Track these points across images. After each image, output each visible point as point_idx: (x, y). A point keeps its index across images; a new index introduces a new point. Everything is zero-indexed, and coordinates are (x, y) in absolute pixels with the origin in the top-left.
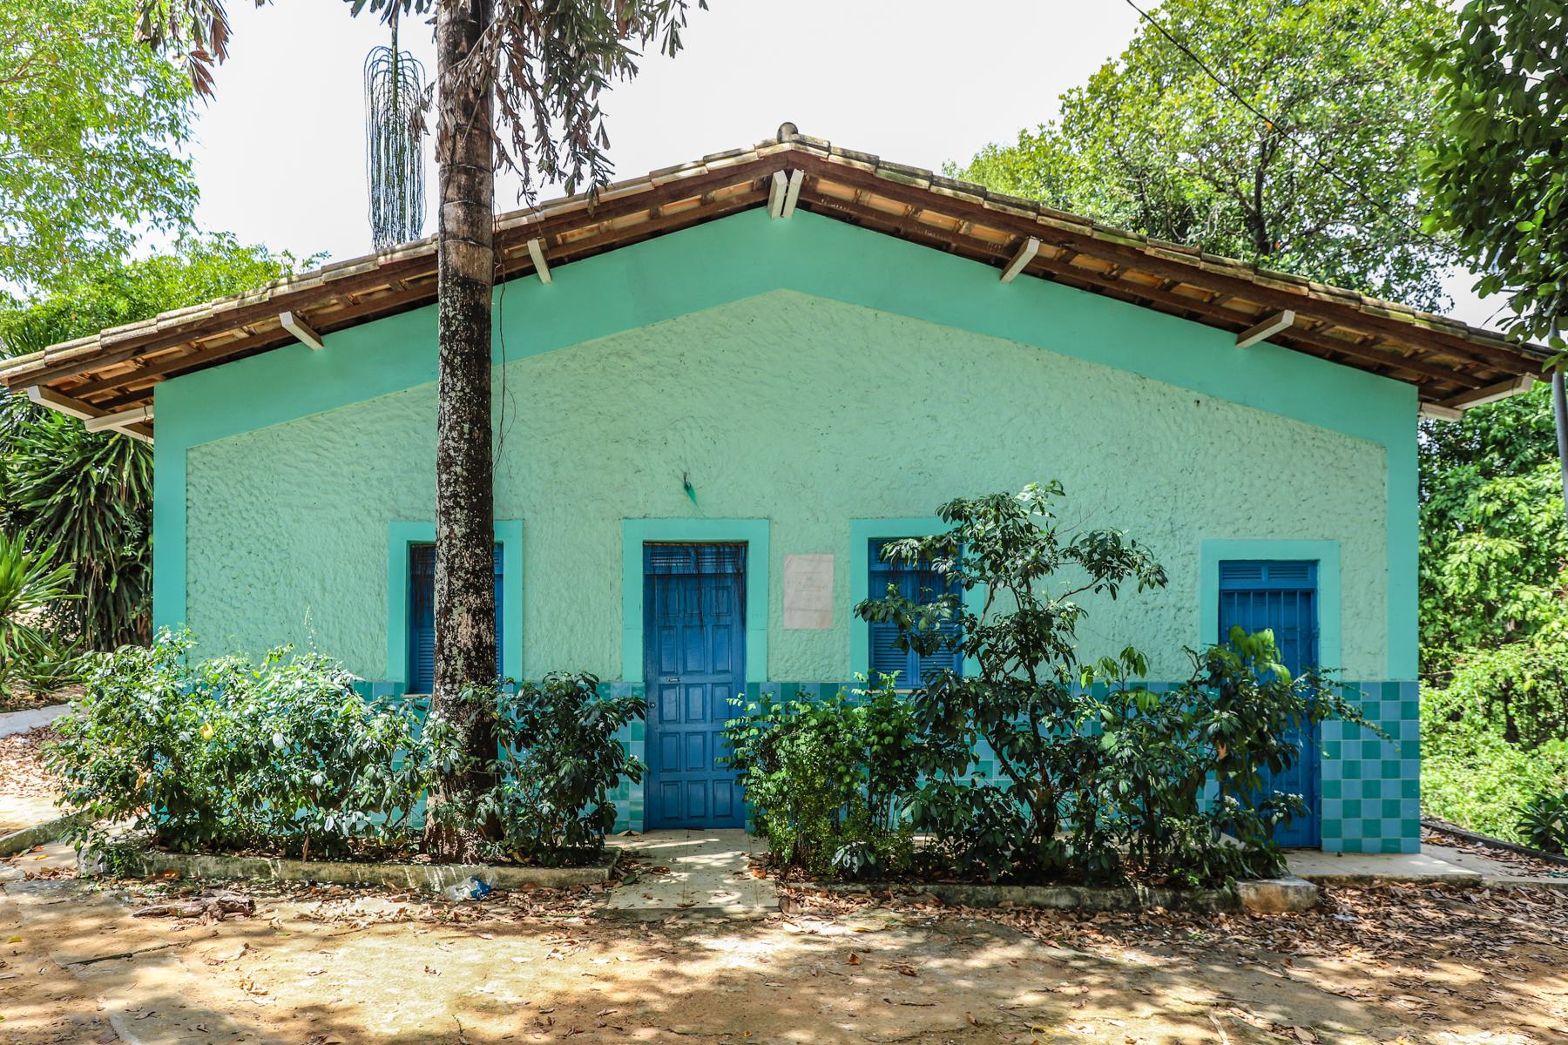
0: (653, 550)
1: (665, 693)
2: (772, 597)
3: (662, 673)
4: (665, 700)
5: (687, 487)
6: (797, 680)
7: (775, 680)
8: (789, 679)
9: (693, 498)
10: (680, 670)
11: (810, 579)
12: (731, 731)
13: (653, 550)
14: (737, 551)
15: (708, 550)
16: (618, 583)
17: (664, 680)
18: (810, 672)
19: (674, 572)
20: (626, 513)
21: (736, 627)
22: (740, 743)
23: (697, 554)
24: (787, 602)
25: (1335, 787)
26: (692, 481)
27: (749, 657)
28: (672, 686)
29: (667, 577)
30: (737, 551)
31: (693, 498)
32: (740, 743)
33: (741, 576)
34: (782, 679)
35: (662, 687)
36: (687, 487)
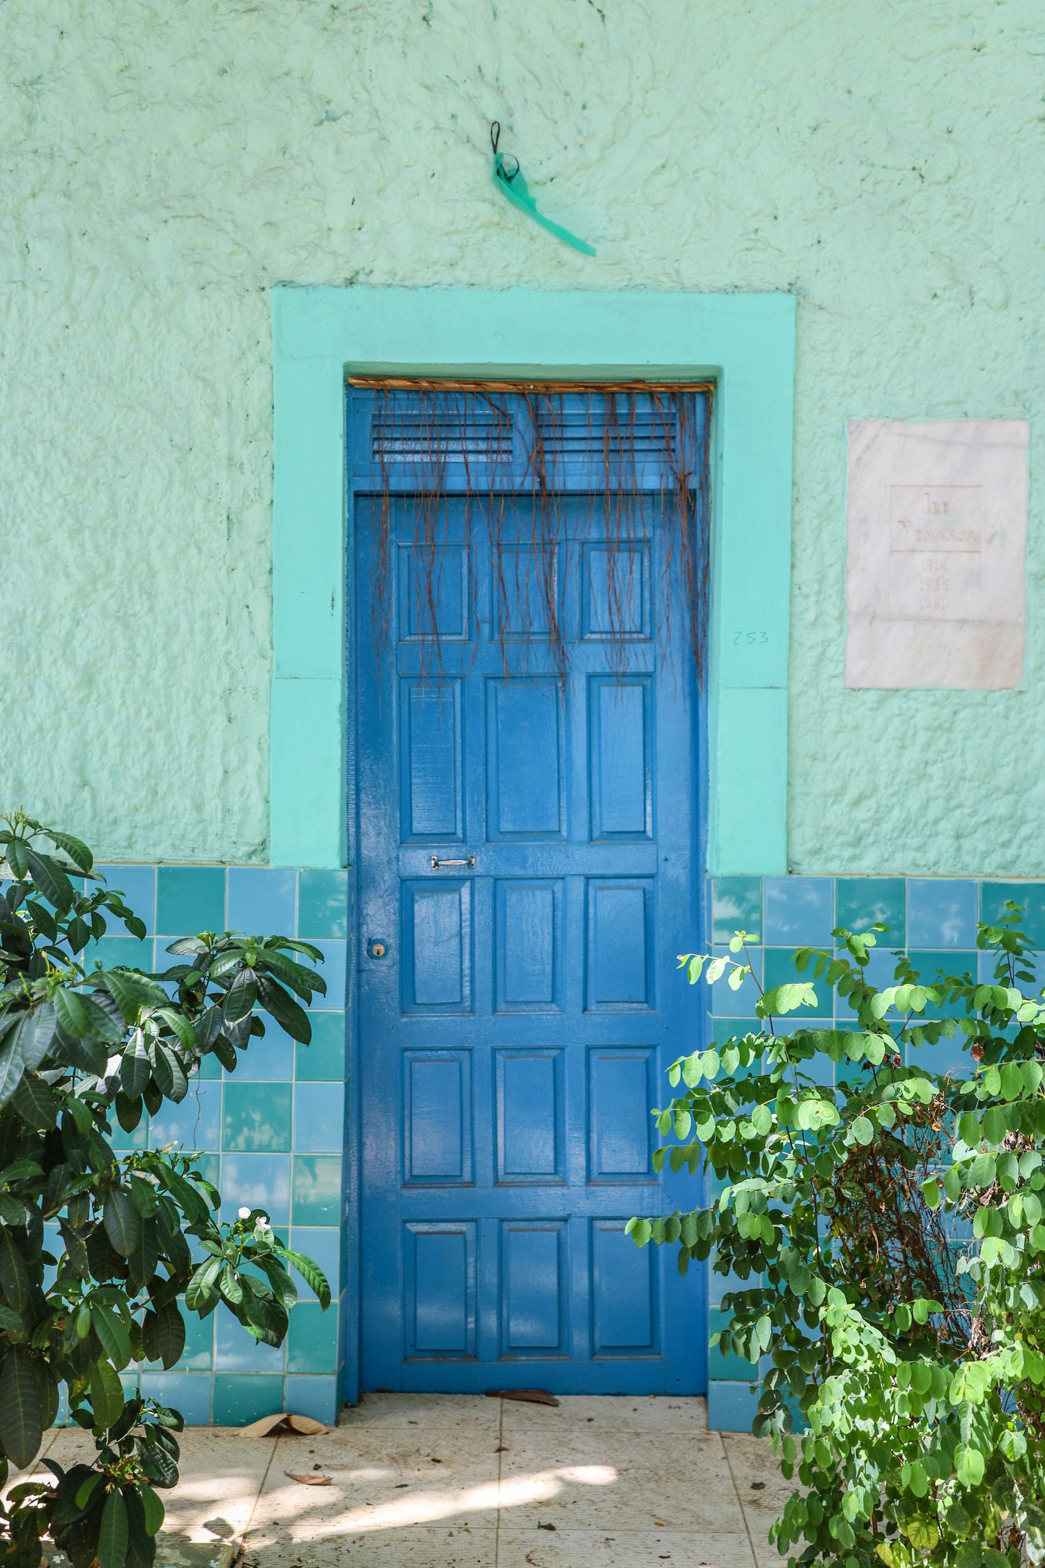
0: (383, 403)
1: (423, 908)
2: (806, 573)
3: (407, 836)
4: (423, 931)
5: (506, 176)
6: (893, 868)
7: (813, 868)
8: (867, 865)
9: (529, 207)
10: (476, 831)
11: (943, 508)
12: (703, 1103)
13: (383, 403)
14: (684, 404)
15: (572, 409)
16: (254, 516)
17: (420, 862)
18: (945, 842)
19: (456, 483)
20: (284, 265)
21: (671, 682)
22: (736, 1159)
23: (538, 421)
24: (857, 590)
25: (65, 829)
26: (525, 151)
27: (344, 993)
28: (446, 884)
29: (428, 501)
30: (684, 404)
31: (529, 207)
32: (736, 1159)
33: (688, 504)
34: (837, 865)
35: (409, 889)
36: (506, 176)
